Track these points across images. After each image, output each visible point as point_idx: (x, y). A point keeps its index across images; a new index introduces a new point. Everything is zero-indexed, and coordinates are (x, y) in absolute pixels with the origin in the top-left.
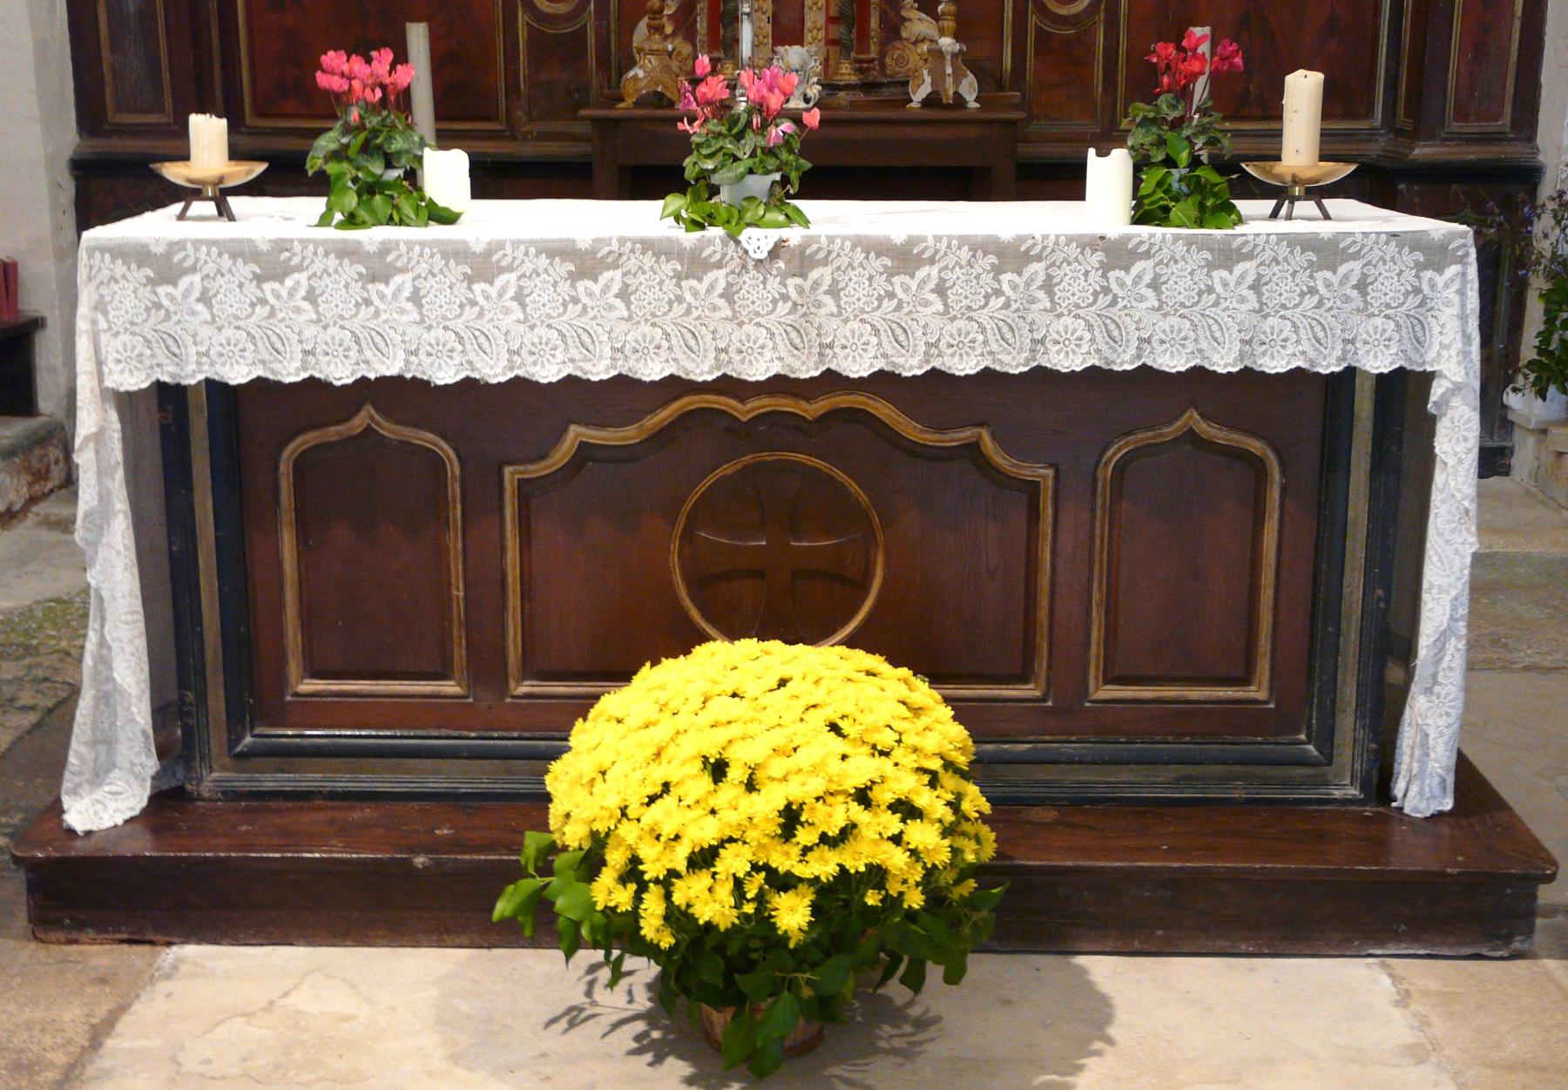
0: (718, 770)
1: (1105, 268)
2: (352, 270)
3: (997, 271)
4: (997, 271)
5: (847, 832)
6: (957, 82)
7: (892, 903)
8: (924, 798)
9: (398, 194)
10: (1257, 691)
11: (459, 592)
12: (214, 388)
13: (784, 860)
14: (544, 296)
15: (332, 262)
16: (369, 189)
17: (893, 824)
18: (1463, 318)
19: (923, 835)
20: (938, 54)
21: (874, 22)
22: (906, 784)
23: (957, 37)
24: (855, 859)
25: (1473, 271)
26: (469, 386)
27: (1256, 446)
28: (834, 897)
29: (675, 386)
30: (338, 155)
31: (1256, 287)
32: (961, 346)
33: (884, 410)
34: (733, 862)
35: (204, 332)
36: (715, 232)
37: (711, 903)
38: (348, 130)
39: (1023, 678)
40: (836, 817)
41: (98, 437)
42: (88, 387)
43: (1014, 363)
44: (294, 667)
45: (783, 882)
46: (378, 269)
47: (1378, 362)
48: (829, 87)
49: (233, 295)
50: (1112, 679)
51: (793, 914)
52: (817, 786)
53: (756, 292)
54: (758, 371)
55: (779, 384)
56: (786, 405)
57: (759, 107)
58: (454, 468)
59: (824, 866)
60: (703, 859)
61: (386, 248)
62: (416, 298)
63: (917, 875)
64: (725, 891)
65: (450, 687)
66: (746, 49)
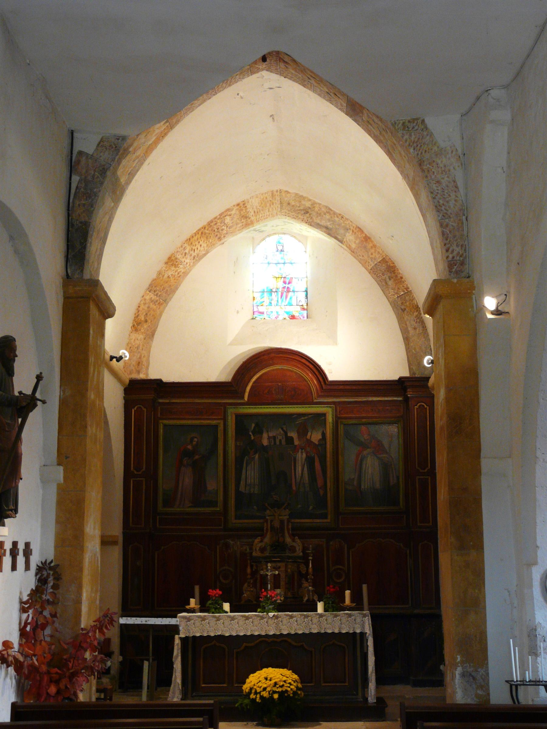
0: (266, 679)
1: (319, 618)
2: (215, 619)
3: (304, 618)
4: (304, 618)
5: (283, 685)
6: (313, 596)
8: (293, 683)
9: (220, 610)
10: (347, 684)
11: (227, 670)
12: (194, 637)
13: (275, 689)
14: (241, 623)
15: (212, 618)
16: (216, 609)
17: (289, 685)
18: (369, 624)
19: (292, 687)
20: (309, 590)
21: (296, 584)
23: (313, 586)
25: (370, 618)
26: (230, 636)
27: (343, 645)
28: (281, 694)
29: (259, 636)
30: (212, 604)
31: (340, 620)
32: (300, 629)
33: (289, 640)
34: (268, 689)
35: (194, 629)
36: (265, 613)
37: (265, 694)
38: (212, 600)
39: (311, 682)
40: (282, 684)
41: (178, 644)
43: (307, 632)
44: (201, 682)
45: (275, 692)
46: (218, 619)
47: (358, 631)
48: (286, 598)
49: (198, 623)
50: (325, 682)
51: (276, 696)
52: (279, 680)
54: (271, 633)
55: (274, 635)
56: (275, 640)
57: (271, 596)
58: (227, 650)
59: (280, 690)
60: (265, 689)
61: (219, 616)
62: (223, 623)
63: (292, 692)
64: (267, 693)
65: (225, 685)
66: (269, 588)
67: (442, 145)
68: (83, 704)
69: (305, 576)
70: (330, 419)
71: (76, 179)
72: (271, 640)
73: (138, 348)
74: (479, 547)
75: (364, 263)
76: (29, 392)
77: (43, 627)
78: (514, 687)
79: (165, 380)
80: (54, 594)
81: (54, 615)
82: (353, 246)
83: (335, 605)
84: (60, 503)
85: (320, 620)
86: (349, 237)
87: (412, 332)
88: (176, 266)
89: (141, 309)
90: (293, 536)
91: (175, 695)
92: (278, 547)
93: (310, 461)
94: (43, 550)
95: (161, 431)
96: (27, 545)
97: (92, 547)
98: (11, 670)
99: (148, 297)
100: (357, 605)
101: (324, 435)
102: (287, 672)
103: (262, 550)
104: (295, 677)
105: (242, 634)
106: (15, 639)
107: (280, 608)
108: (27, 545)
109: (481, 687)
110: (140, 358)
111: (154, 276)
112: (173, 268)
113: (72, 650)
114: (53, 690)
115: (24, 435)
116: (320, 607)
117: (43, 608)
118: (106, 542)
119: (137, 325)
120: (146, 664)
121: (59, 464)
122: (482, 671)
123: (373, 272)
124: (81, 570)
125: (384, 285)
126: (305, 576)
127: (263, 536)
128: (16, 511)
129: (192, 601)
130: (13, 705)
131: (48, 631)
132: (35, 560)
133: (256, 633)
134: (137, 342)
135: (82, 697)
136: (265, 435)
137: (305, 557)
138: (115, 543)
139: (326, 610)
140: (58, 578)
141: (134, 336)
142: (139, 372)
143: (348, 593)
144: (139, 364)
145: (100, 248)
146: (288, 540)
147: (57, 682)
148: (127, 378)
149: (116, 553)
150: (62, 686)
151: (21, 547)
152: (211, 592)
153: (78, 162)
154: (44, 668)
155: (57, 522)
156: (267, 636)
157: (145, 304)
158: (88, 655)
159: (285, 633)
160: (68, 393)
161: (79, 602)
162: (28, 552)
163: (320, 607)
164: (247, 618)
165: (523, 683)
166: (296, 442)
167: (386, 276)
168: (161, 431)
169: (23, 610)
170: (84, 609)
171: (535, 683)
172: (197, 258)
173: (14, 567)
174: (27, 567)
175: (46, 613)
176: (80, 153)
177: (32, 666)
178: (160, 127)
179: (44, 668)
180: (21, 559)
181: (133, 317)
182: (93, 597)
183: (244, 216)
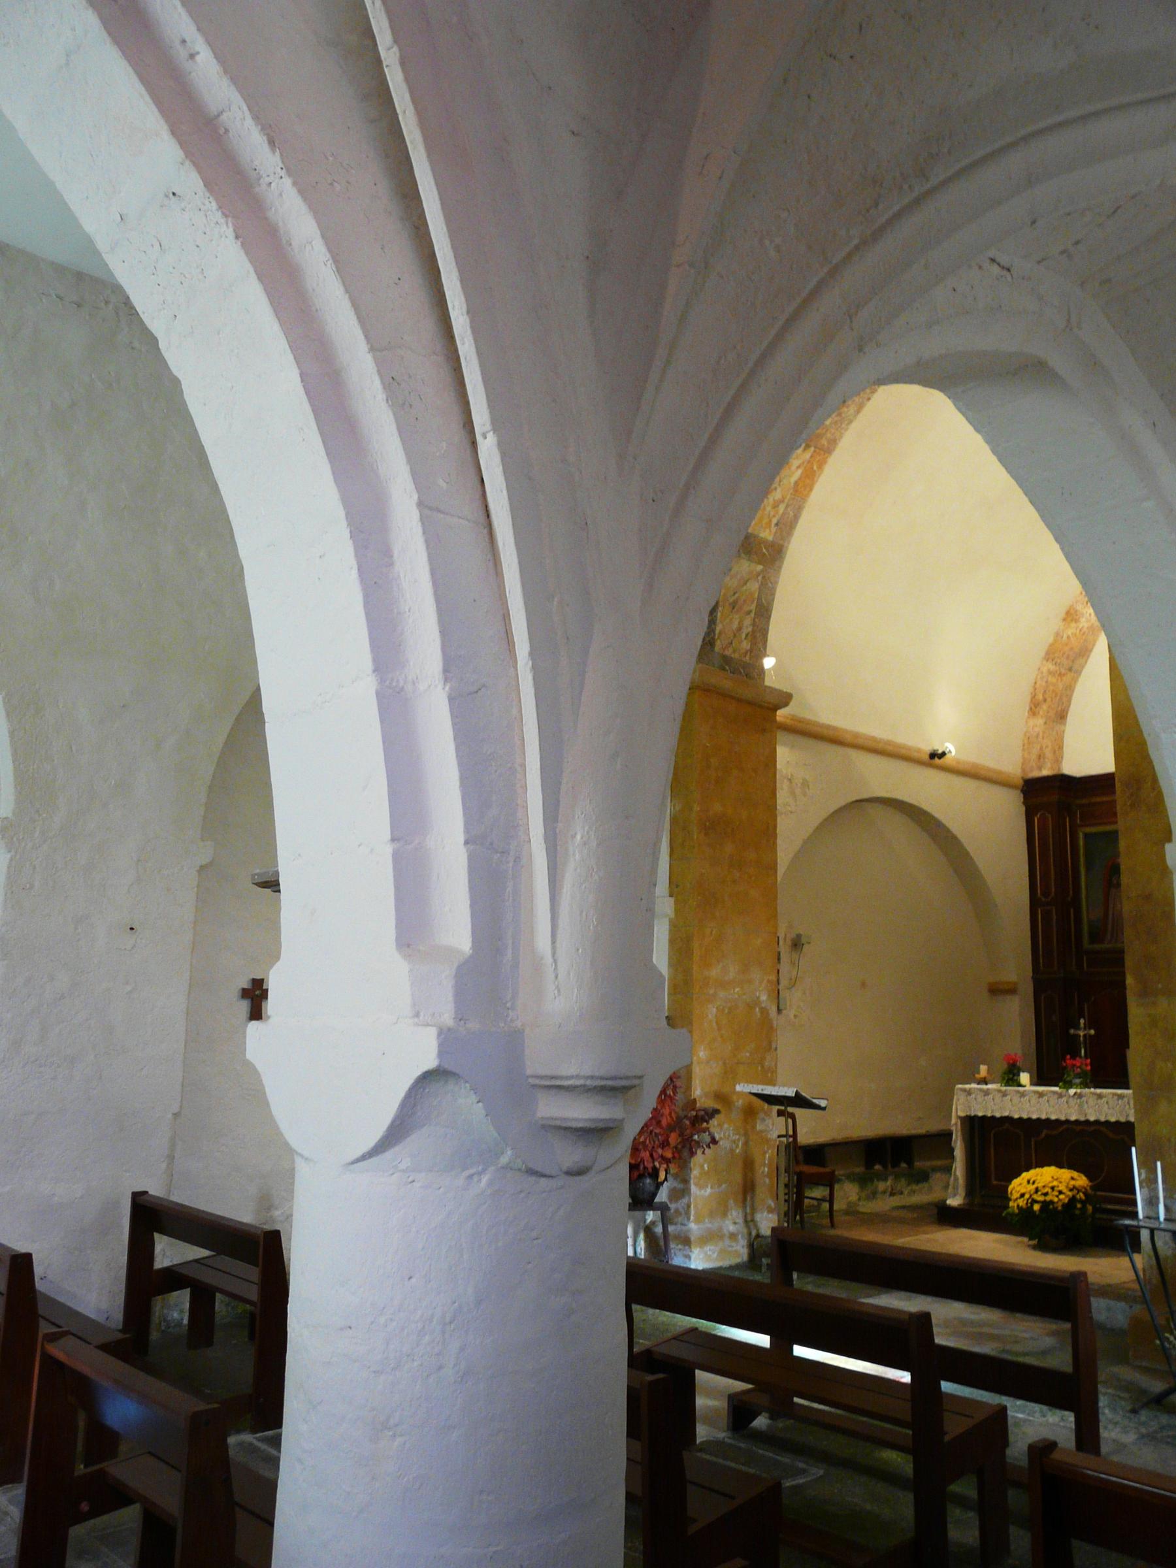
7: (1055, 1209)
13: (1035, 1197)
14: (1033, 1101)
22: (1062, 1188)
24: (1048, 1198)
26: (1020, 1119)
32: (1112, 1115)
33: (1103, 1129)
34: (1027, 1196)
42: (1166, 1243)
51: (1036, 1207)
53: (1072, 1102)
54: (1073, 1118)
55: (1076, 1121)
59: (1041, 1198)
60: (1022, 1195)
72: (1092, 1128)
73: (1037, 736)
88: (1077, 621)
89: (1038, 686)
95: (1081, 843)
99: (1045, 670)
102: (1065, 1174)
105: (1034, 1117)
110: (1041, 749)
111: (1051, 640)
112: (1073, 625)
133: (1053, 1117)
134: (1036, 729)
138: (1011, 990)
141: (1032, 722)
142: (1040, 768)
144: (1039, 757)
156: (1067, 1121)
157: (1042, 678)
159: (1092, 1119)
160: (678, 808)
164: (1100, 1096)
168: (1081, 843)
171: (749, 1218)
178: (800, 458)
181: (1028, 699)
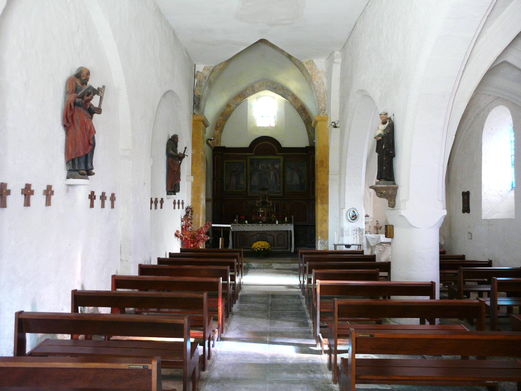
37: (259, 249)
67: (319, 69)
68: (201, 249)
69: (273, 213)
70: (282, 160)
71: (196, 80)
74: (327, 203)
75: (294, 107)
76: (182, 153)
77: (188, 226)
78: (335, 246)
79: (226, 146)
80: (191, 217)
81: (191, 223)
82: (291, 101)
83: (282, 222)
84: (192, 188)
85: (278, 227)
86: (290, 98)
87: (310, 131)
90: (269, 199)
91: (230, 247)
92: (264, 203)
93: (275, 175)
94: (188, 203)
96: (183, 201)
97: (203, 202)
98: (179, 239)
100: (289, 222)
101: (280, 167)
103: (259, 204)
104: (268, 244)
106: (180, 230)
107: (264, 223)
108: (183, 201)
109: (326, 246)
113: (197, 234)
114: (192, 245)
115: (181, 166)
116: (277, 222)
117: (188, 221)
118: (207, 200)
119: (217, 128)
120: (221, 239)
121: (192, 175)
122: (326, 242)
123: (298, 110)
124: (200, 209)
125: (301, 114)
126: (273, 213)
127: (259, 200)
128: (179, 190)
129: (235, 220)
130: (181, 249)
131: (190, 228)
132: (185, 206)
135: (201, 248)
136: (260, 166)
137: (273, 207)
138: (210, 201)
139: (279, 223)
140: (192, 212)
143: (286, 218)
145: (306, 372)
146: (267, 201)
147: (193, 243)
148: (213, 146)
149: (210, 204)
150: (195, 244)
151: (181, 202)
152: (242, 217)
153: (197, 75)
154: (189, 239)
155: (192, 194)
158: (202, 235)
161: (199, 219)
162: (183, 203)
163: (277, 222)
165: (338, 245)
166: (271, 168)
167: (302, 112)
169: (182, 221)
170: (201, 221)
172: (237, 105)
173: (179, 208)
174: (183, 208)
175: (189, 222)
176: (198, 72)
177: (185, 238)
179: (189, 239)
180: (181, 205)
182: (200, 220)
183: (252, 90)
